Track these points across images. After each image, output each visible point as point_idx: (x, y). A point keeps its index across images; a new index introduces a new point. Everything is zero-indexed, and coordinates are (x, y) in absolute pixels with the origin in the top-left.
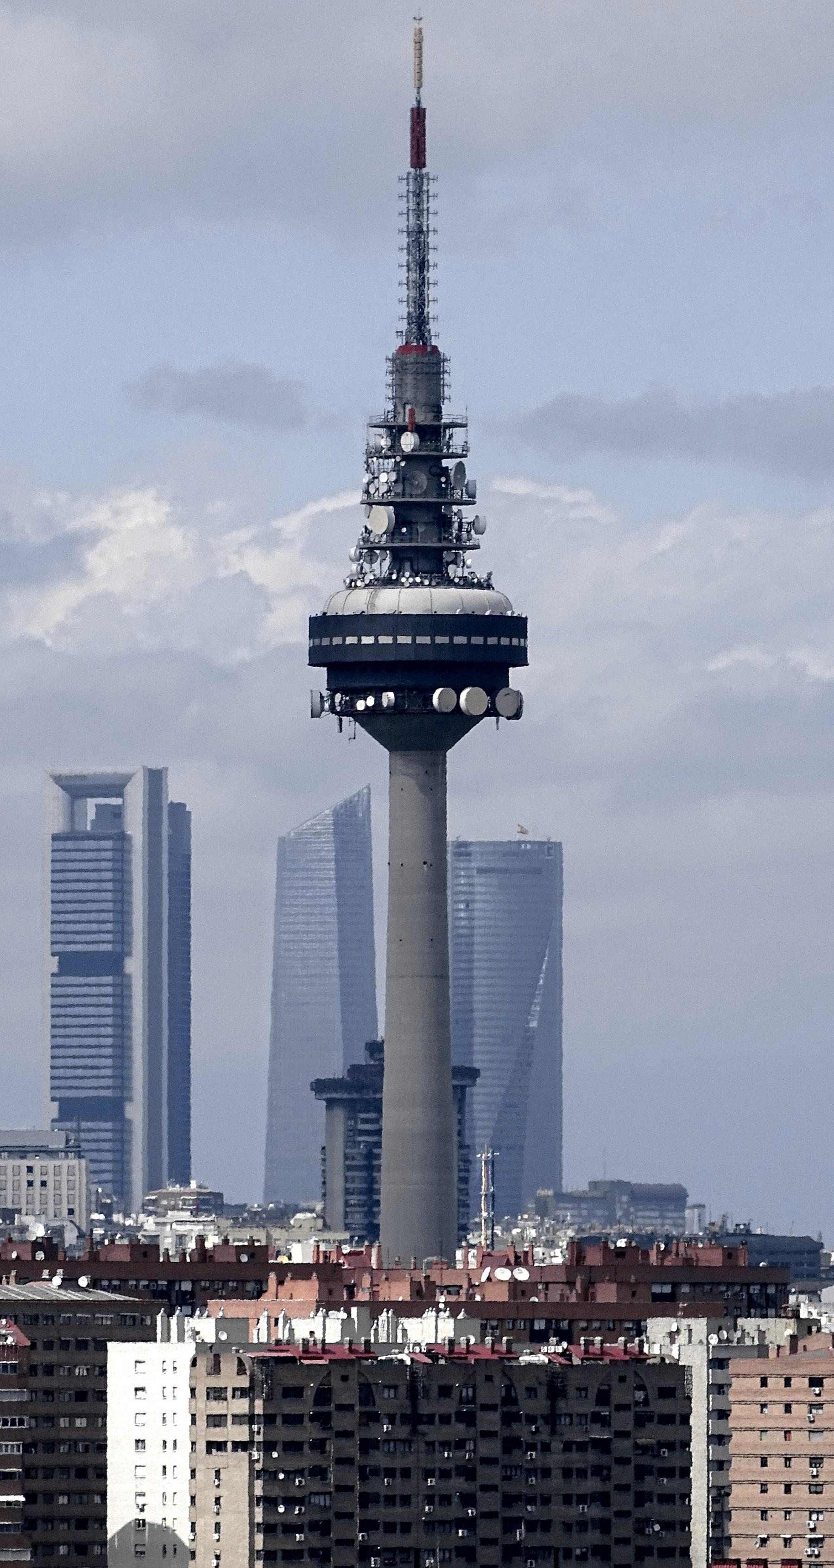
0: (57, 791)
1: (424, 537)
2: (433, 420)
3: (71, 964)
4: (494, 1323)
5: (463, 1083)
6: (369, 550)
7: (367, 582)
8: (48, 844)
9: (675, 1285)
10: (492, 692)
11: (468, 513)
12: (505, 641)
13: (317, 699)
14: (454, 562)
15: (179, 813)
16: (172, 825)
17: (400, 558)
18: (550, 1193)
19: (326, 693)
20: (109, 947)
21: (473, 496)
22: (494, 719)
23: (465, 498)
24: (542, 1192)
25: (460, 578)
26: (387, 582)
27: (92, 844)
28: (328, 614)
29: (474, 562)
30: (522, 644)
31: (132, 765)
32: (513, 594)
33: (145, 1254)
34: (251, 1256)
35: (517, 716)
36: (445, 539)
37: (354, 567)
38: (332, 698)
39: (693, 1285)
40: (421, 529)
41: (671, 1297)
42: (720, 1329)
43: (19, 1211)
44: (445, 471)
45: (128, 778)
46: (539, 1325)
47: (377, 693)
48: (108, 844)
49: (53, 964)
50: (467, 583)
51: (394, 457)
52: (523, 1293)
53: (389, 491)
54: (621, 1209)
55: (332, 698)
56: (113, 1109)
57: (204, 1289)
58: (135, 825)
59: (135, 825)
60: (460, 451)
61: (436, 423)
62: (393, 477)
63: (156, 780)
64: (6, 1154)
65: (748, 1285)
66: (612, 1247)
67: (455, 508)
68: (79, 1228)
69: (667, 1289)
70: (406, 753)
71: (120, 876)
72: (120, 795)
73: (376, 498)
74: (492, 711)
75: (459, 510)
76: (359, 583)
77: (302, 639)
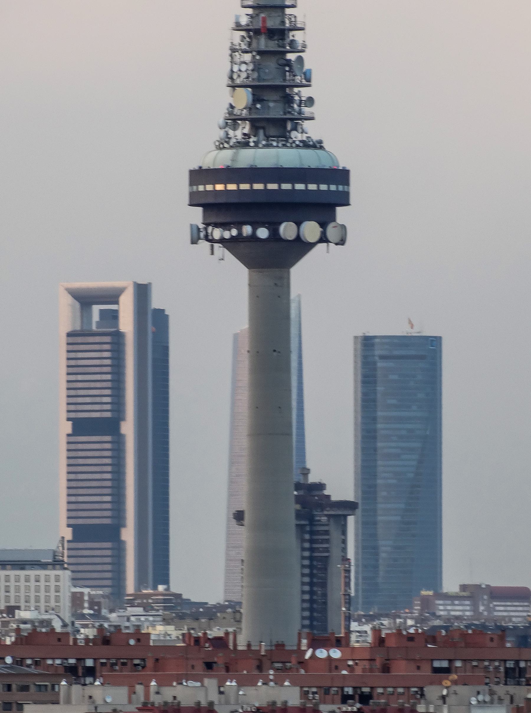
0: (69, 299)
1: (275, 110)
2: (280, 24)
3: (81, 427)
4: (314, 690)
5: (345, 512)
6: (233, 120)
7: (231, 144)
8: (64, 339)
9: (451, 661)
10: (323, 225)
11: (305, 93)
12: (323, 187)
13: (195, 231)
14: (295, 129)
15: (161, 318)
16: (154, 325)
17: (257, 125)
18: (431, 593)
19: (201, 226)
20: (108, 415)
21: (309, 80)
22: (325, 244)
23: (304, 82)
24: (424, 593)
25: (300, 141)
26: (245, 145)
27: (97, 339)
28: (204, 168)
29: (312, 130)
30: (346, 190)
31: (125, 282)
32: (340, 152)
33: (59, 640)
34: (138, 640)
35: (342, 242)
36: (289, 112)
37: (222, 133)
38: (206, 229)
39: (464, 661)
40: (271, 104)
41: (447, 671)
42: (478, 693)
43: (18, 608)
44: (288, 63)
45: (120, 291)
46: (349, 691)
47: (255, 225)
48: (108, 339)
49: (68, 427)
50: (306, 145)
51: (251, 52)
52: (336, 668)
53: (248, 78)
54: (483, 605)
55: (206, 229)
56: (111, 533)
57: (103, 664)
58: (127, 324)
59: (127, 324)
60: (300, 48)
61: (282, 27)
62: (251, 67)
63: (142, 292)
64: (9, 566)
65: (505, 661)
66: (404, 633)
67: (296, 90)
68: (63, 621)
69: (445, 664)
70: (260, 270)
71: (118, 361)
72: (117, 303)
73: (238, 82)
74: (324, 239)
75: (299, 91)
76: (226, 145)
77: (184, 189)
